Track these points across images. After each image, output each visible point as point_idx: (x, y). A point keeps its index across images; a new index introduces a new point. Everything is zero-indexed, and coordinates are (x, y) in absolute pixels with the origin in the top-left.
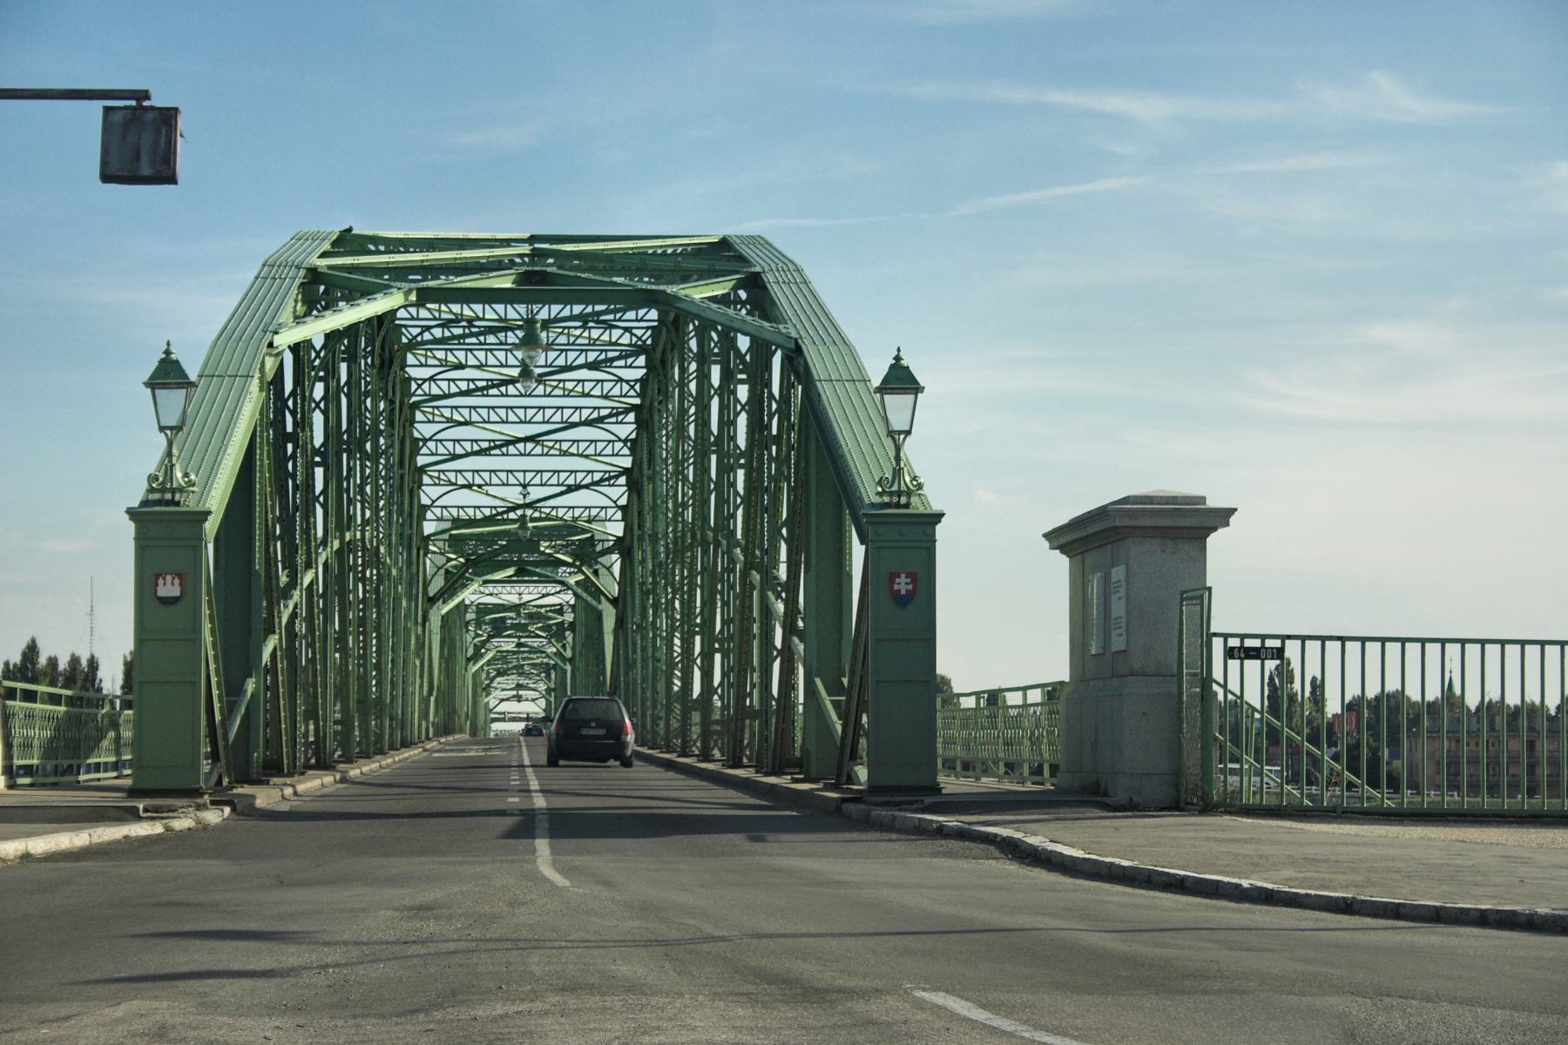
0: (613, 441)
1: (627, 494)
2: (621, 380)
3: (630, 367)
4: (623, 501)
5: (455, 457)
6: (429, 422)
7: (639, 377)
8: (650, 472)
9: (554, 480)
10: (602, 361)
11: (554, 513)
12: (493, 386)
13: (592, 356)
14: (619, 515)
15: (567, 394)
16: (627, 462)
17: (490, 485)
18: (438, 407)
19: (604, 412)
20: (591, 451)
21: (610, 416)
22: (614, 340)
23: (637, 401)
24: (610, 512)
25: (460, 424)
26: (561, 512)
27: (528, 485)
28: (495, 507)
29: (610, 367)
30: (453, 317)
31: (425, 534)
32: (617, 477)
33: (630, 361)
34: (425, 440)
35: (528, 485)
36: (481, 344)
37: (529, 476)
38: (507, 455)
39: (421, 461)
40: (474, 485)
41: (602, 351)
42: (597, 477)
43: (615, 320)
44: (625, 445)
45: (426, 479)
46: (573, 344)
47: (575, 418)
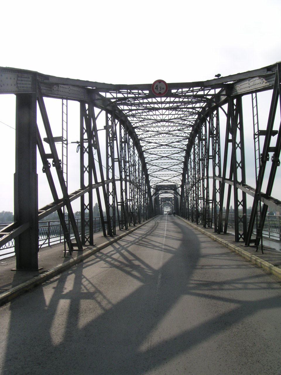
2: (185, 133)
4: (183, 167)
5: (152, 161)
9: (170, 164)
10: (179, 141)
11: (169, 135)
12: (159, 158)
13: (179, 128)
14: (182, 170)
16: (184, 160)
19: (179, 151)
21: (181, 152)
23: (186, 149)
24: (181, 169)
25: (154, 166)
29: (183, 130)
30: (143, 120)
32: (182, 163)
33: (185, 140)
34: (143, 146)
36: (151, 126)
39: (143, 150)
41: (181, 127)
42: (178, 163)
43: (186, 119)
46: (175, 125)
47: (174, 153)
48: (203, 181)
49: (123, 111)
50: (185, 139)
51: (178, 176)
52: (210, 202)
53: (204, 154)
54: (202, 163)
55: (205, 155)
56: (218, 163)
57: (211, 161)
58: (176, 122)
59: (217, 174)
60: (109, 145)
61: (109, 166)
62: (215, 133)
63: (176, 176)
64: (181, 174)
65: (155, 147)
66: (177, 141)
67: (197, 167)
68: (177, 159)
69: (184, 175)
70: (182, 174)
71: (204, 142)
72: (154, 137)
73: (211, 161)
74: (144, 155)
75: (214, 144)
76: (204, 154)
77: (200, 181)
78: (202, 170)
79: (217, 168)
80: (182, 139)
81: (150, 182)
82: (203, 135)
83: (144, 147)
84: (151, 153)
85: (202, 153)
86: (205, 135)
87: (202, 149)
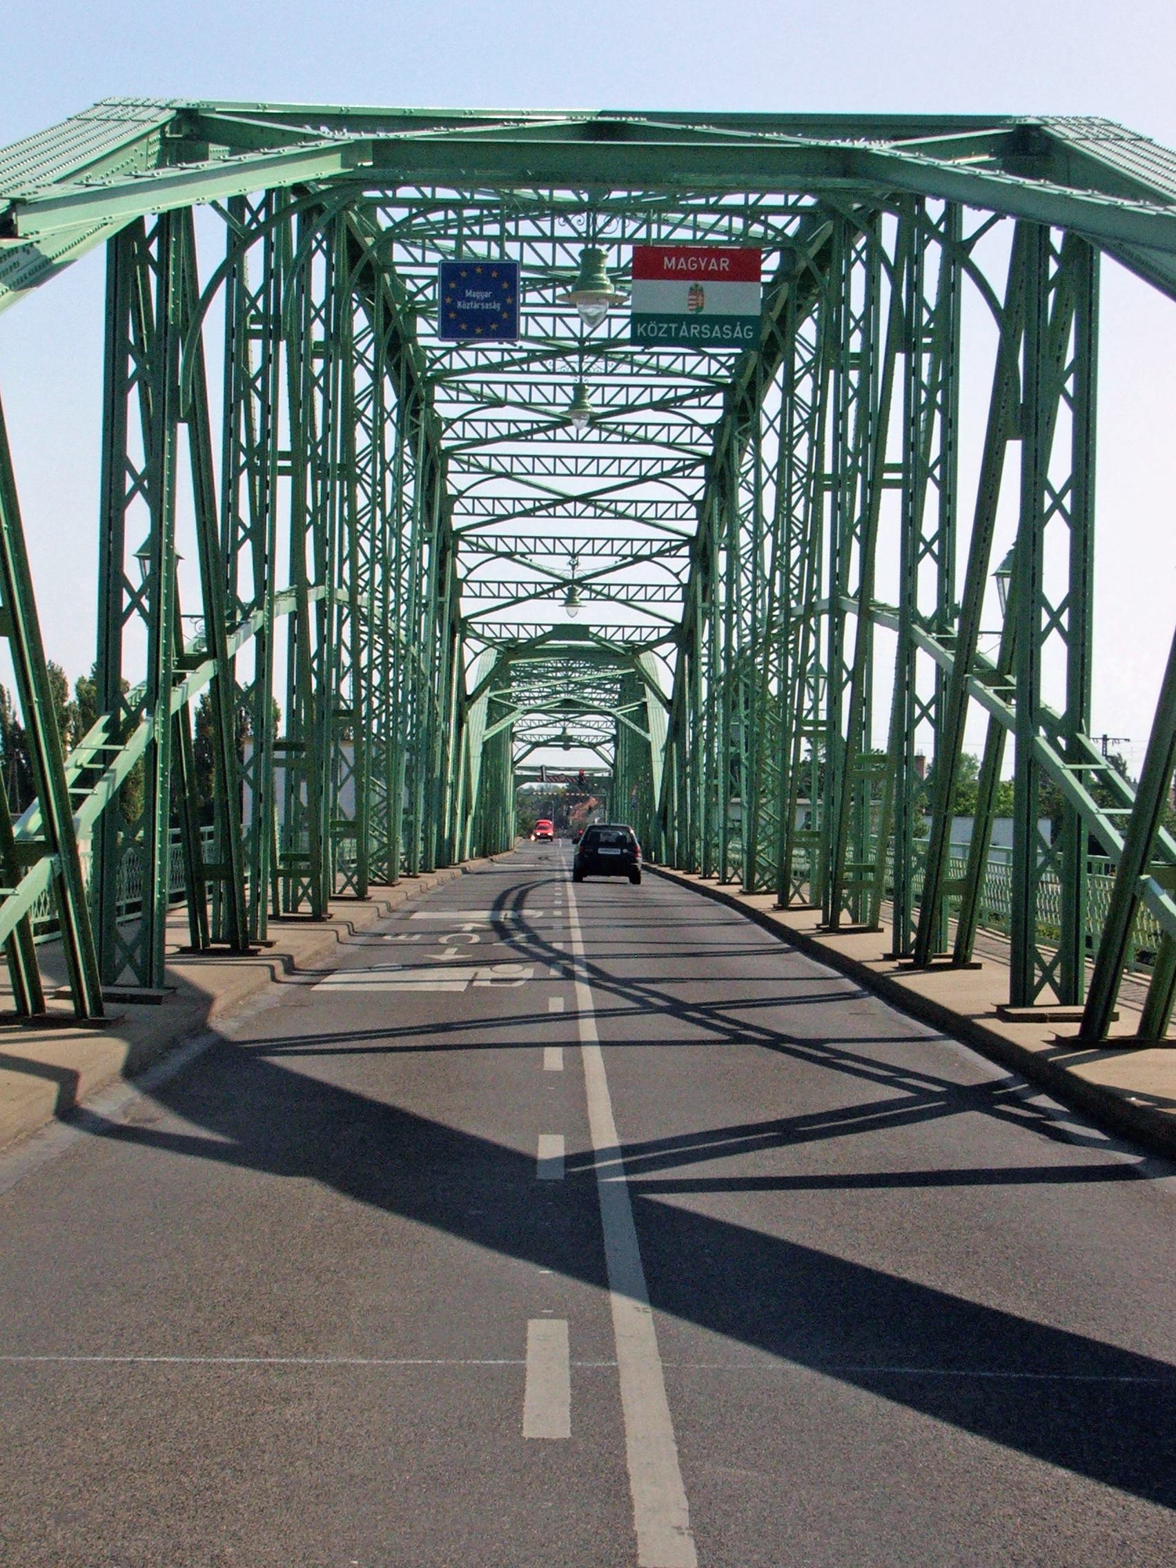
1: (689, 568)
3: (705, 407)
4: (699, 497)
6: (452, 401)
7: (713, 421)
8: (707, 605)
9: (613, 470)
10: (671, 400)
12: (539, 430)
14: (693, 512)
15: (628, 439)
16: (691, 528)
17: (535, 553)
18: (474, 455)
20: (650, 514)
22: (688, 369)
23: (709, 451)
24: (682, 508)
25: (499, 475)
27: (578, 554)
28: (540, 583)
29: (680, 407)
31: (462, 616)
32: (693, 467)
33: (704, 400)
34: (450, 423)
35: (578, 554)
37: (579, 544)
38: (555, 516)
39: (444, 444)
40: (516, 553)
42: (668, 466)
45: (462, 546)
48: (837, 628)
50: (705, 394)
51: (660, 553)
53: (850, 445)
54: (836, 506)
55: (858, 452)
56: (939, 536)
57: (891, 502)
58: (644, 371)
59: (927, 604)
60: (311, 523)
63: (646, 551)
65: (521, 434)
66: (656, 398)
67: (799, 512)
70: (690, 541)
71: (854, 376)
72: (523, 372)
73: (891, 502)
75: (917, 414)
76: (850, 445)
77: (812, 621)
78: (835, 553)
79: (927, 570)
80: (689, 391)
81: (466, 590)
82: (852, 324)
83: (458, 426)
85: (839, 437)
87: (840, 416)
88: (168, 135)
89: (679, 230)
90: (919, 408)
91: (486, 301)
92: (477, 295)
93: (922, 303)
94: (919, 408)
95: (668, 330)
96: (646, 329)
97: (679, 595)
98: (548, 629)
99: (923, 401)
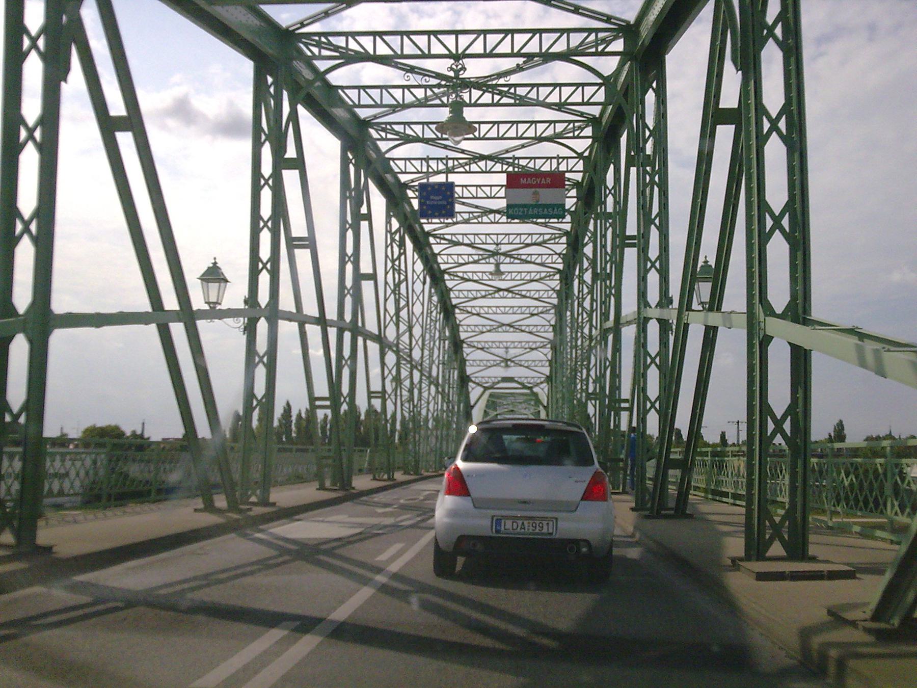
0: (552, 255)
4: (558, 288)
12: (483, 259)
23: (561, 267)
25: (474, 314)
26: (523, 162)
37: (509, 344)
42: (543, 275)
44: (560, 256)
47: (528, 241)
49: (340, 91)
51: (542, 313)
52: (623, 405)
57: (631, 255)
61: (262, 218)
62: (649, 148)
64: (553, 308)
68: (538, 261)
69: (560, 311)
74: (457, 316)
81: (461, 329)
84: (465, 276)
86: (615, 191)
88: (621, 491)
89: (504, 98)
90: (647, 185)
91: (440, 200)
92: (436, 198)
93: (645, 126)
94: (645, 185)
95: (523, 212)
96: (513, 212)
97: (547, 364)
98: (500, 379)
99: (648, 180)
